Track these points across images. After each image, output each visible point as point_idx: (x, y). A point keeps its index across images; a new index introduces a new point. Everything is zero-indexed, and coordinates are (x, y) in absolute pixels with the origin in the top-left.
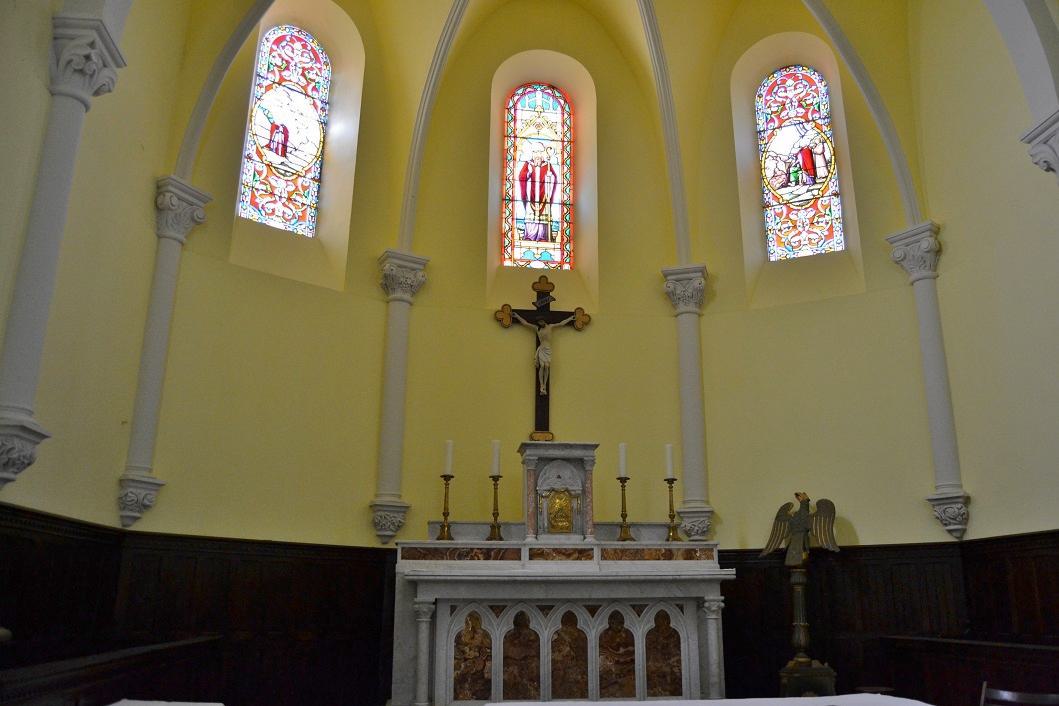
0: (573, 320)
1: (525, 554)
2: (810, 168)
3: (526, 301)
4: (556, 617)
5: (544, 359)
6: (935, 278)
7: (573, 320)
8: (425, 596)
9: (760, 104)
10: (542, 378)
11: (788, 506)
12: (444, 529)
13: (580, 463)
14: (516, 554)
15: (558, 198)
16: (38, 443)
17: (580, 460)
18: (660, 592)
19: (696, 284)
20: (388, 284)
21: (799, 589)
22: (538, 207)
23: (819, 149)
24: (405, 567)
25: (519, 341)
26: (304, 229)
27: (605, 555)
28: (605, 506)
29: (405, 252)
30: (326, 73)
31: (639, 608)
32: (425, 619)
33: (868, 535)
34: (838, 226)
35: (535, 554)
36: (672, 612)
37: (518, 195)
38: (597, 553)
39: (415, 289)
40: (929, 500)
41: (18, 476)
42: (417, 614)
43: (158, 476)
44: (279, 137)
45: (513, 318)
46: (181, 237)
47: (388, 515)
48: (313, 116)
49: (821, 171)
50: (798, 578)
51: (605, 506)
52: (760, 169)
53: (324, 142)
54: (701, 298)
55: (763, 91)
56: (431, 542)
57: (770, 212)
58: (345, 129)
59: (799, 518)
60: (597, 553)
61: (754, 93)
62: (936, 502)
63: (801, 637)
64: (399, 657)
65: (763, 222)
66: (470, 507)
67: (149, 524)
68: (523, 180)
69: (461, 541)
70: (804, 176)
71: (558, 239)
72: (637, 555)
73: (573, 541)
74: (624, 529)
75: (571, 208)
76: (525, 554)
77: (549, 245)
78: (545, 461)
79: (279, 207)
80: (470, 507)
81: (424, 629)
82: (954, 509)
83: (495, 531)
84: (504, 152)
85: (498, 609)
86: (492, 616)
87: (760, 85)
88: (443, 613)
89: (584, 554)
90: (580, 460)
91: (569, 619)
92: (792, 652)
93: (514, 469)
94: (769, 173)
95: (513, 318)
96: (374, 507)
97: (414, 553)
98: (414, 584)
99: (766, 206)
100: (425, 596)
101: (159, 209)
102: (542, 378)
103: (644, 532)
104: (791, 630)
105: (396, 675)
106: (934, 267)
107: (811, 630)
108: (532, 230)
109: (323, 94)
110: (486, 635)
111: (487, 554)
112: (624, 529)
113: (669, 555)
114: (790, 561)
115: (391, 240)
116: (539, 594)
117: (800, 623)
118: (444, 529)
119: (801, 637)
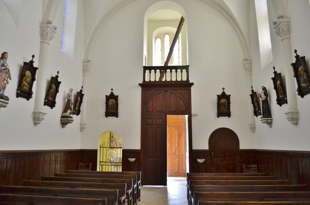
40: (285, 114)
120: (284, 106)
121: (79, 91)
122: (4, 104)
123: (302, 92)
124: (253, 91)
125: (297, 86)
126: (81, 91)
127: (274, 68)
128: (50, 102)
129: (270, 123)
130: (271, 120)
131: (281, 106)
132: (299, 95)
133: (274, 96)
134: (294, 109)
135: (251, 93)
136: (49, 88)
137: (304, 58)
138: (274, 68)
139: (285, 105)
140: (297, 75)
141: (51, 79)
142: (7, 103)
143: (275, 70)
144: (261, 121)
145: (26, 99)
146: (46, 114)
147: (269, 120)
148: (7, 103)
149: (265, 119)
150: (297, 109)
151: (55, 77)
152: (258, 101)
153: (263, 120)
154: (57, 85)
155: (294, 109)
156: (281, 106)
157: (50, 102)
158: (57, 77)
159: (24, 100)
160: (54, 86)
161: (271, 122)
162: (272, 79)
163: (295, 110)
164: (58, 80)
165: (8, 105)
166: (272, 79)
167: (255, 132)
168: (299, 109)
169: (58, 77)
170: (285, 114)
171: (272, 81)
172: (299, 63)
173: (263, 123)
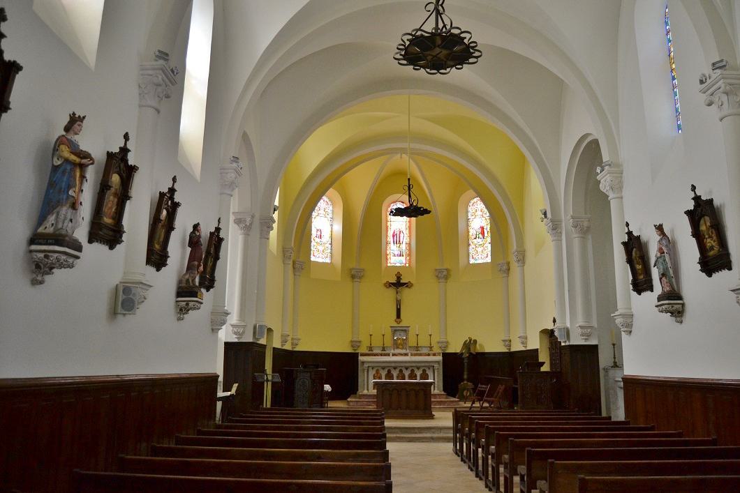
0: (408, 285)
1: (391, 355)
2: (483, 233)
3: (394, 280)
4: (398, 370)
5: (399, 298)
6: (508, 276)
7: (408, 285)
8: (366, 365)
9: (470, 209)
10: (398, 303)
11: (466, 341)
12: (371, 348)
13: (405, 331)
14: (389, 355)
15: (404, 243)
16: (147, 290)
17: (405, 331)
18: (423, 364)
19: (444, 273)
20: (353, 277)
21: (466, 364)
22: (398, 245)
23: (485, 227)
24: (361, 358)
25: (392, 291)
26: (328, 261)
27: (412, 355)
28: (412, 342)
29: (358, 267)
30: (331, 208)
31: (418, 368)
32: (366, 371)
33: (488, 349)
34: (490, 254)
35: (393, 355)
36: (427, 369)
37: (392, 241)
38: (409, 354)
39: (360, 278)
40: (733, 291)
41: (47, 278)
42: (364, 370)
43: (299, 337)
44: (319, 233)
45: (390, 285)
46: (229, 193)
47: (355, 344)
48: (328, 223)
49: (486, 235)
50: (466, 361)
51: (412, 342)
52: (468, 232)
53: (332, 232)
54: (446, 278)
55: (471, 204)
56: (367, 352)
57: (470, 247)
58: (338, 228)
59: (469, 344)
60: (409, 354)
61: (467, 205)
62: (504, 341)
63: (465, 377)
64: (360, 380)
65: (468, 250)
66: (377, 342)
67: (297, 349)
68: (393, 236)
69: (375, 352)
70: (481, 236)
71: (405, 256)
72: (421, 355)
73: (404, 351)
74: (417, 348)
75: (409, 244)
76: (391, 355)
77: (401, 258)
78: (396, 330)
79: (321, 255)
80: (377, 342)
81: (366, 373)
82: (507, 343)
83: (384, 350)
84: (387, 227)
85: (383, 368)
86: (382, 370)
87: (470, 202)
88: (370, 369)
89: (406, 355)
90: (405, 331)
91: (401, 371)
92: (463, 380)
93: (388, 332)
94: (470, 234)
95: (390, 285)
96: (352, 341)
97: (363, 355)
98: (363, 363)
99: (470, 245)
100: (366, 365)
101: (294, 268)
102: (398, 303)
103: (424, 349)
104: (463, 374)
105: (359, 383)
106: (508, 274)
107: (468, 375)
108: (396, 253)
109: (330, 215)
110: (381, 375)
111: (381, 355)
112: (417, 348)
113: (429, 355)
114: (464, 356)
115: (353, 265)
116: (393, 365)
117: (465, 373)
118: (371, 348)
119: (465, 377)
120: (721, 276)
121: (213, 230)
122: (71, 260)
123: (709, 266)
124: (630, 233)
125: (631, 278)
126: (218, 229)
127: (694, 188)
128: (157, 258)
129: (679, 312)
130: (680, 306)
131: (710, 275)
132: (634, 290)
133: (689, 252)
134: (627, 308)
135: (626, 239)
136: (155, 221)
137: (638, 237)
138: (694, 188)
139: (725, 272)
140: (697, 234)
141: (108, 158)
142: (78, 257)
143: (695, 193)
144: (657, 306)
145: (107, 247)
146: (151, 286)
147: (676, 306)
148: (78, 257)
149: (667, 302)
150: (526, 333)
151: (117, 150)
152: (644, 259)
153: (663, 304)
154: (124, 175)
155: (627, 308)
156: (710, 275)
157: (157, 258)
158: (124, 151)
159: (153, 270)
160: (115, 179)
161: (681, 310)
162: (688, 213)
163: (629, 311)
164: (127, 161)
165: (78, 260)
166: (688, 213)
167: (631, 332)
168: (634, 311)
169: (129, 151)
170: (733, 291)
171: (686, 219)
172: (702, 210)
173: (662, 312)
